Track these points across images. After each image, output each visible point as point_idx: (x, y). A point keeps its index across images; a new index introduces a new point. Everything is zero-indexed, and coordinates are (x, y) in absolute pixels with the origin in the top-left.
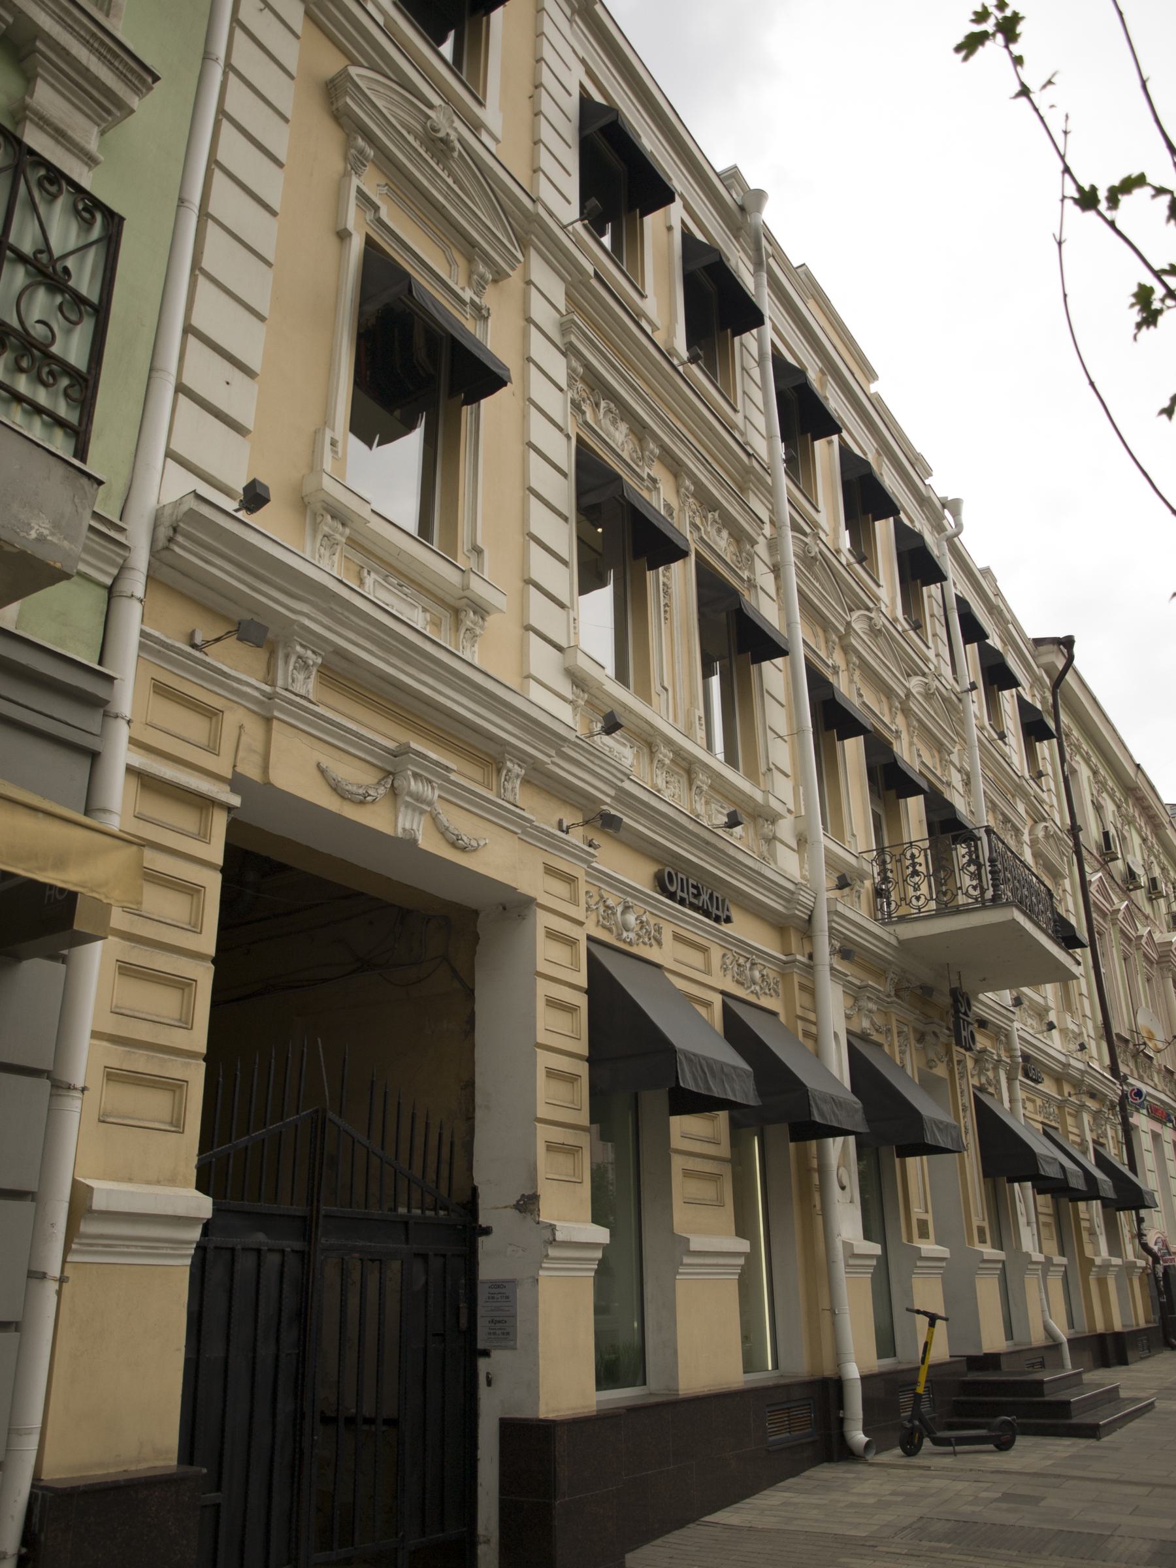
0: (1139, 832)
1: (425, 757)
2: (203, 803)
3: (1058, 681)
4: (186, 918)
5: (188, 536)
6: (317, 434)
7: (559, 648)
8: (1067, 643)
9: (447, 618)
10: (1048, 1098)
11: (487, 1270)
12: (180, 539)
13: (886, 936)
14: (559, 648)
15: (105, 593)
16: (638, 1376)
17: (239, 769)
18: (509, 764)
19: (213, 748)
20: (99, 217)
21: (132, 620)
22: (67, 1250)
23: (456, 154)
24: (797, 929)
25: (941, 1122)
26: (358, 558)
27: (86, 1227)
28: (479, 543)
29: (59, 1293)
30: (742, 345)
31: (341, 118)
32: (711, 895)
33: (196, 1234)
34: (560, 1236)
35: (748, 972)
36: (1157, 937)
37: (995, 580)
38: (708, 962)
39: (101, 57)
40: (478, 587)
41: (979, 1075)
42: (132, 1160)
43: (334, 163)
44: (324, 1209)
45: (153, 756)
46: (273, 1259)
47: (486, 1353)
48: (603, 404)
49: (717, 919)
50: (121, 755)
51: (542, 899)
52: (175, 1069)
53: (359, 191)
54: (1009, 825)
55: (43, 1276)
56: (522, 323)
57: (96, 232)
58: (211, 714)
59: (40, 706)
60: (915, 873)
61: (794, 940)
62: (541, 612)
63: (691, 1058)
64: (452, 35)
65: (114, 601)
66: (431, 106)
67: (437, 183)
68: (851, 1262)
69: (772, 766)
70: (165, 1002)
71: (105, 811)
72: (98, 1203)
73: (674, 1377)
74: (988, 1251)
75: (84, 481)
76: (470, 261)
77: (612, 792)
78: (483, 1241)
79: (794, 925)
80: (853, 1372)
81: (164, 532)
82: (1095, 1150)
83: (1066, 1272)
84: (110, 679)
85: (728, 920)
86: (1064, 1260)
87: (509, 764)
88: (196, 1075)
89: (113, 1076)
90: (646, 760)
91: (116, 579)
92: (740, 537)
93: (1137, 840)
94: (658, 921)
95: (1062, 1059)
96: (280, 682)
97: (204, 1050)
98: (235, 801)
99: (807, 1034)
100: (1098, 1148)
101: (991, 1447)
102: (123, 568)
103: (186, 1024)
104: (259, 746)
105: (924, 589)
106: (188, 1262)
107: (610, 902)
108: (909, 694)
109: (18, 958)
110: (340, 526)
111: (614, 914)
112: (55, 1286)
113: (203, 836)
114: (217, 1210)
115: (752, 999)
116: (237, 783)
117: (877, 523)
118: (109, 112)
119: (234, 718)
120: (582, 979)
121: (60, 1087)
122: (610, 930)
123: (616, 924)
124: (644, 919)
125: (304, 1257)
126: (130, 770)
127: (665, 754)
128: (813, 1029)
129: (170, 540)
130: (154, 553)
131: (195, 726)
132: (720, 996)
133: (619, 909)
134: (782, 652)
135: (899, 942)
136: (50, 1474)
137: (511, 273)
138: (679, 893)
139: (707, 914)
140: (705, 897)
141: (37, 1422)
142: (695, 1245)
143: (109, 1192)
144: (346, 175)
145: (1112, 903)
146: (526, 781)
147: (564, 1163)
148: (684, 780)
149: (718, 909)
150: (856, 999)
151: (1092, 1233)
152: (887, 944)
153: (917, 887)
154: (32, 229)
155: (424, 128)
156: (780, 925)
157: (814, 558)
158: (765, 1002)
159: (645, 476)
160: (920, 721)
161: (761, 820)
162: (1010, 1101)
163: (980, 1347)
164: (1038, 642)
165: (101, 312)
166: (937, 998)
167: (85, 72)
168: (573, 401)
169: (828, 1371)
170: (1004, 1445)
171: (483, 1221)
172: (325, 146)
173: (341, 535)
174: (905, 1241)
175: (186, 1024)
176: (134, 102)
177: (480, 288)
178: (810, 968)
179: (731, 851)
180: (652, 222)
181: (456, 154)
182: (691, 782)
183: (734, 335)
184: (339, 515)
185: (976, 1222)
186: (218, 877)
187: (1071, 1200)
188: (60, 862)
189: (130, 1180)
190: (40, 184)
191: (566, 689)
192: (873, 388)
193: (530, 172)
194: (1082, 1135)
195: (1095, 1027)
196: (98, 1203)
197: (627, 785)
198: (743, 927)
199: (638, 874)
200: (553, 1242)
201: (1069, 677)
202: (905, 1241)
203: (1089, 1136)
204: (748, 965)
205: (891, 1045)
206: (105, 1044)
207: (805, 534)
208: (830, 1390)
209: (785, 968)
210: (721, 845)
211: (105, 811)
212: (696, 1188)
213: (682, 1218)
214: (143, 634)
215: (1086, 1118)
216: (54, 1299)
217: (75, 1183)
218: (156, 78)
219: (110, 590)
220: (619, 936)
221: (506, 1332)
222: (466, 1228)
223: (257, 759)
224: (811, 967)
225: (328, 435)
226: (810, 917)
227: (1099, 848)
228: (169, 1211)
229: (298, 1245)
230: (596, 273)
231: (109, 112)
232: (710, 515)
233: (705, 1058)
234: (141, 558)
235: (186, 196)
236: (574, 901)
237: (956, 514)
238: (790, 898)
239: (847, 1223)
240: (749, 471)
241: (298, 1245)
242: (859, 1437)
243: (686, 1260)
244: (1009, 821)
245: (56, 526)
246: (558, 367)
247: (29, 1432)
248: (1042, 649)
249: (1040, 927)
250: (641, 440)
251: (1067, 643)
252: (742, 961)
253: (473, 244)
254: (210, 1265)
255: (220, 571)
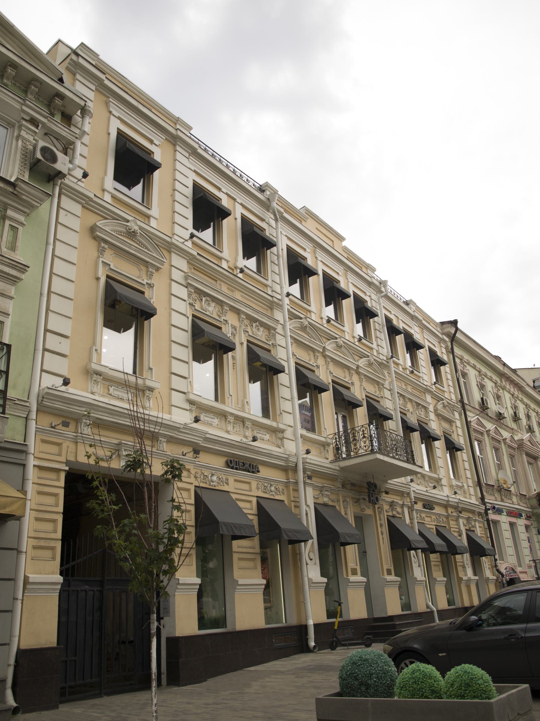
0: (509, 392)
1: (127, 444)
2: (58, 471)
3: (453, 338)
4: (54, 503)
5: (47, 398)
7: (184, 393)
10: (439, 515)
12: (45, 400)
13: (333, 467)
14: (184, 393)
15: (25, 419)
16: (224, 625)
17: (68, 459)
18: (160, 439)
19: (60, 455)
21: (33, 425)
22: (23, 593)
23: (139, 234)
24: (292, 470)
25: (350, 534)
26: (107, 383)
27: (28, 587)
29: (22, 603)
30: (271, 252)
31: (96, 238)
32: (250, 464)
34: (180, 582)
35: (269, 488)
37: (415, 304)
38: (250, 487)
39: (12, 268)
42: (41, 568)
43: (95, 254)
44: (106, 578)
45: (42, 461)
48: (204, 299)
49: (253, 472)
50: (32, 462)
52: (52, 544)
53: (103, 262)
54: (420, 406)
55: (17, 599)
56: (169, 281)
58: (59, 445)
59: (7, 456)
61: (290, 474)
62: (177, 383)
63: (225, 524)
64: (142, 180)
65: (28, 421)
66: (128, 221)
68: (312, 585)
69: (282, 412)
70: (49, 526)
71: (28, 479)
73: (235, 625)
75: (5, 419)
77: (202, 440)
79: (288, 468)
80: (311, 622)
81: (40, 398)
82: (467, 534)
83: (477, 582)
84: (26, 445)
85: (258, 471)
87: (160, 439)
89: (35, 547)
90: (223, 422)
91: (28, 415)
92: (268, 328)
93: (507, 396)
94: (226, 476)
96: (79, 431)
97: (61, 538)
98: (67, 468)
99: (295, 506)
100: (470, 533)
101: (364, 646)
102: (29, 411)
103: (55, 531)
104: (74, 451)
105: (371, 320)
106: (58, 594)
107: (206, 474)
108: (358, 367)
109: (7, 522)
110: (99, 377)
111: (208, 477)
112: (21, 601)
113: (58, 480)
114: (64, 580)
115: (272, 497)
116: (67, 463)
118: (16, 282)
120: (192, 501)
121: (19, 552)
122: (206, 483)
123: (209, 480)
124: (220, 477)
125: (101, 592)
126: (34, 466)
127: (231, 419)
129: (42, 401)
130: (38, 404)
131: (54, 449)
132: (256, 498)
133: (210, 476)
135: (341, 468)
136: (23, 646)
137: (162, 267)
138: (235, 466)
139: (249, 471)
141: (17, 633)
143: (34, 577)
144: (99, 257)
146: (168, 442)
148: (242, 425)
149: (253, 469)
150: (321, 491)
151: (464, 567)
155: (126, 230)
156: (285, 469)
159: (222, 320)
161: (277, 432)
162: (410, 519)
163: (387, 613)
164: (442, 323)
167: (8, 274)
168: (189, 304)
170: (368, 645)
173: (99, 379)
174: (345, 576)
175: (55, 531)
176: (23, 276)
178: (296, 483)
180: (225, 222)
181: (139, 234)
182: (244, 425)
183: (267, 249)
185: (385, 567)
186: (63, 490)
187: (452, 554)
189: (41, 574)
191: (187, 406)
192: (344, 244)
193: (172, 224)
194: (459, 528)
195: (473, 482)
197: (208, 436)
198: (264, 472)
199: (219, 462)
200: (179, 584)
201: (458, 335)
202: (345, 576)
203: (463, 529)
204: (269, 486)
205: (339, 506)
206: (32, 539)
207: (301, 318)
208: (303, 629)
210: (251, 448)
211: (28, 479)
213: (237, 573)
214: (36, 428)
215: (461, 521)
216: (20, 605)
218: (28, 267)
223: (74, 455)
224: (297, 483)
226: (296, 465)
227: (480, 404)
228: (51, 581)
231: (16, 282)
233: (232, 523)
234: (34, 408)
235: (42, 292)
237: (385, 287)
238: (287, 460)
239: (313, 572)
240: (273, 302)
241: (99, 589)
242: (312, 644)
243: (238, 587)
244: (420, 404)
246: (183, 292)
247: (15, 636)
248: (444, 326)
250: (222, 306)
252: (266, 485)
255: (58, 405)
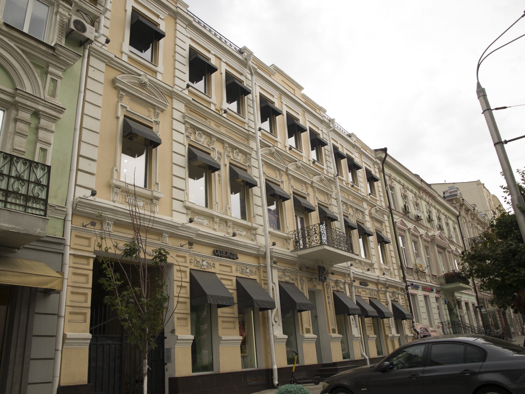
0: (425, 201)
2: (88, 258)
3: (384, 161)
6: (113, 168)
7: (182, 201)
8: (385, 150)
9: (149, 202)
10: (372, 290)
11: (166, 346)
13: (293, 255)
14: (182, 201)
19: (89, 246)
20: (46, 168)
21: (69, 225)
27: (66, 341)
28: (157, 182)
31: (116, 88)
33: (89, 341)
34: (179, 338)
36: (430, 234)
37: (356, 136)
38: (231, 270)
40: (156, 194)
41: (337, 286)
46: (114, 346)
47: (166, 364)
48: (197, 132)
49: (233, 259)
50: (68, 251)
51: (176, 263)
52: (84, 310)
53: (121, 105)
55: (58, 350)
56: (171, 119)
57: (46, 171)
60: (316, 233)
62: (176, 194)
66: (140, 75)
67: (143, 94)
70: (81, 298)
72: (68, 337)
73: (219, 369)
74: (337, 335)
76: (155, 109)
78: (166, 340)
79: (260, 256)
80: (275, 367)
81: (75, 205)
84: (64, 239)
85: (237, 258)
86: (399, 335)
88: (89, 312)
89: (71, 313)
90: (212, 222)
93: (424, 203)
95: (377, 278)
102: (66, 215)
103: (86, 301)
105: (323, 148)
107: (198, 260)
108: (312, 182)
109: (50, 294)
117: (302, 134)
119: (94, 239)
120: (188, 280)
121: (59, 316)
128: (266, 282)
134: (327, 145)
136: (62, 384)
140: (229, 254)
141: (58, 375)
142: (223, 339)
144: (118, 102)
145: (407, 227)
147: (183, 322)
150: (284, 272)
151: (390, 327)
152: (294, 257)
153: (316, 237)
154: (34, 176)
156: (257, 257)
157: (274, 153)
158: (251, 277)
160: (318, 189)
162: (350, 293)
165: (48, 186)
166: (318, 269)
168: (186, 136)
169: (270, 368)
171: (165, 336)
172: (113, 95)
174: (301, 334)
176: (61, 116)
177: (157, 115)
179: (236, 242)
182: (227, 225)
183: (245, 96)
184: (118, 187)
186: (92, 272)
188: (47, 284)
190: (35, 167)
191: (184, 211)
192: (303, 92)
195: (397, 266)
196: (68, 337)
198: (242, 259)
199: (208, 252)
200: (177, 339)
201: (388, 159)
202: (301, 334)
203: (389, 300)
205: (297, 283)
208: (270, 372)
209: (258, 268)
210: (232, 241)
212: (226, 325)
213: (221, 332)
217: (64, 333)
218: (65, 109)
219: (64, 220)
220: (201, 268)
221: (169, 359)
222: (161, 338)
225: (115, 169)
227: (403, 210)
229: (119, 343)
230: (193, 99)
232: (235, 151)
234: (70, 212)
236: (186, 262)
237: (333, 123)
239: (277, 331)
240: (249, 135)
241: (119, 343)
242: (276, 382)
245: (41, 229)
246: (181, 128)
249: (335, 248)
250: (211, 138)
251: (385, 150)
253: (155, 105)
254: (94, 348)
